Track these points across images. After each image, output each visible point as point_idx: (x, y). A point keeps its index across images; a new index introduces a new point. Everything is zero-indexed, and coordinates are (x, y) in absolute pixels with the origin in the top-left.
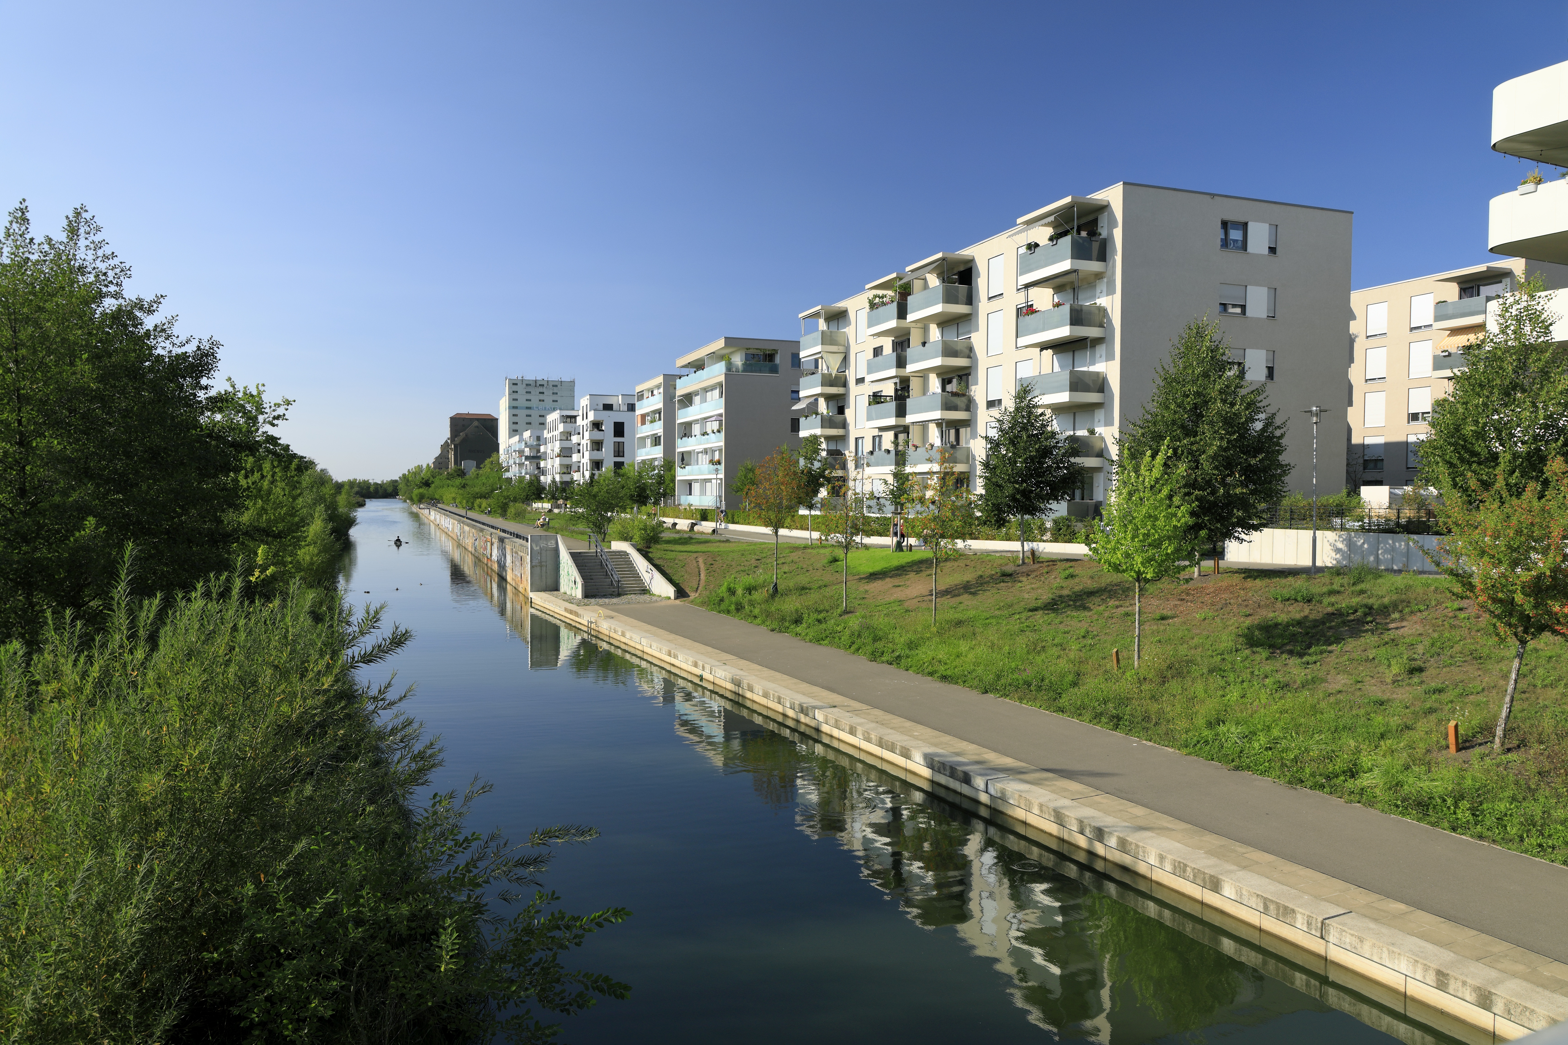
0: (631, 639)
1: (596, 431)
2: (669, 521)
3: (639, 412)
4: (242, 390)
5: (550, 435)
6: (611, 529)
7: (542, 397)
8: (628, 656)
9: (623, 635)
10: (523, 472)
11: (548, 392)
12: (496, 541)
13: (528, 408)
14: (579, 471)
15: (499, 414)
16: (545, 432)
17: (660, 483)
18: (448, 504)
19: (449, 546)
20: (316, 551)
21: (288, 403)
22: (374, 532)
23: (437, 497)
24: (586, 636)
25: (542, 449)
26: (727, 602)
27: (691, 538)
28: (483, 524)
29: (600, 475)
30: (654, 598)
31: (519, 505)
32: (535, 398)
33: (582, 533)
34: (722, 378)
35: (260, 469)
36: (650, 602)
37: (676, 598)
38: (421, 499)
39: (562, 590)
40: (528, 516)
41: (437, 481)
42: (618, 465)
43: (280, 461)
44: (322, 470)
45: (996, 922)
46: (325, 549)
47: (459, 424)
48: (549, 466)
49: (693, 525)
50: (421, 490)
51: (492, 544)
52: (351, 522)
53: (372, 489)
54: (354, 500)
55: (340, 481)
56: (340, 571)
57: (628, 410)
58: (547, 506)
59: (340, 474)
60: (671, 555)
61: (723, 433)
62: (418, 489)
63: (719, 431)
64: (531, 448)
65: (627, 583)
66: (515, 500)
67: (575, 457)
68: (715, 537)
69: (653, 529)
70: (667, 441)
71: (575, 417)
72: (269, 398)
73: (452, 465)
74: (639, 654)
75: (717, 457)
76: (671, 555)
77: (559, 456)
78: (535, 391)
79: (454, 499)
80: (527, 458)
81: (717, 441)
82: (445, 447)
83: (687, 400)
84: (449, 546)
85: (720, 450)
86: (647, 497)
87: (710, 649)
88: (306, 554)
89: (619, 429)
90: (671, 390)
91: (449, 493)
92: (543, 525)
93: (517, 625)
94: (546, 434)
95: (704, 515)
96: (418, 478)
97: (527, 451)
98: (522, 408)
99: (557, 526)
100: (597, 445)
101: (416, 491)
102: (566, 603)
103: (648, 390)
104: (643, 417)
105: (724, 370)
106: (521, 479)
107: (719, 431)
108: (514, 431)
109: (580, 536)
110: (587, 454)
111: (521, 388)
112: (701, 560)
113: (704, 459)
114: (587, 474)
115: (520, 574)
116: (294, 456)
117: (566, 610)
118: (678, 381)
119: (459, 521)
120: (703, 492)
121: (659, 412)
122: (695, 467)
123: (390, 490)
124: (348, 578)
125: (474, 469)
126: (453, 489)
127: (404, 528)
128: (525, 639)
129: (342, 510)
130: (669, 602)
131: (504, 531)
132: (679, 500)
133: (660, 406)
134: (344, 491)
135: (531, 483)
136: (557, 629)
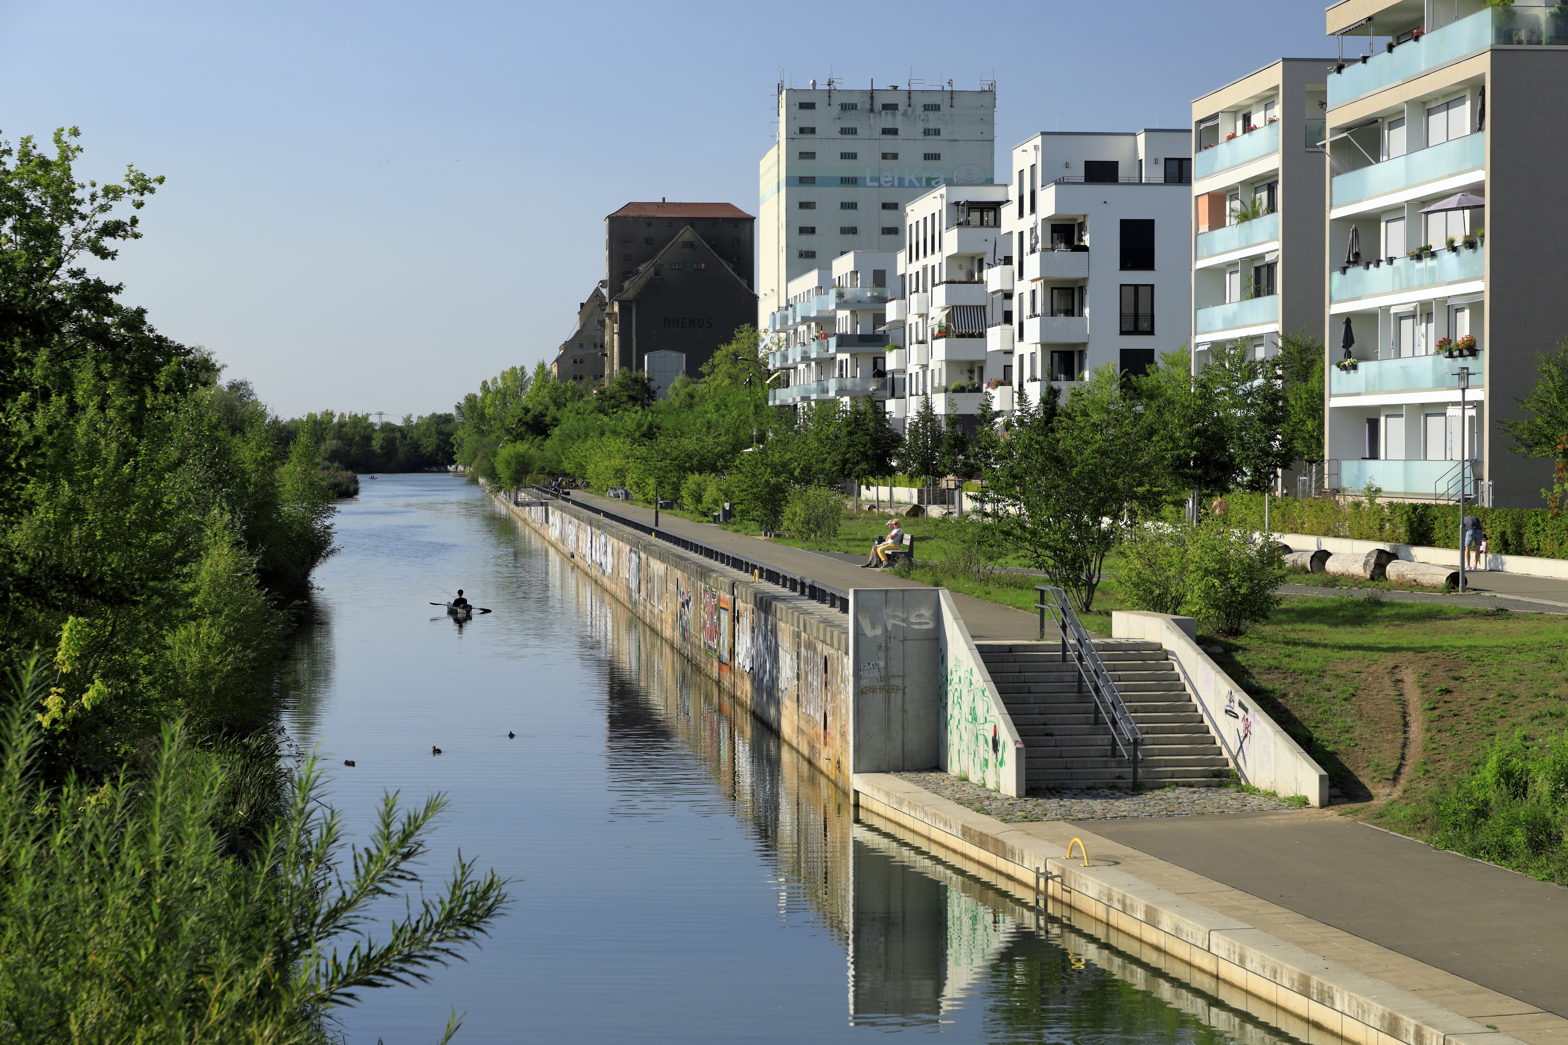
0: (1176, 934)
1: (1062, 254)
2: (1302, 544)
3: (1202, 185)
4: (16, 148)
5: (916, 266)
6: (1113, 570)
7: (889, 144)
8: (1166, 991)
9: (1151, 920)
10: (832, 385)
11: (910, 128)
12: (745, 607)
13: (849, 181)
14: (1006, 381)
15: (757, 203)
16: (902, 257)
17: (1271, 420)
18: (601, 491)
19: (605, 623)
20: (217, 638)
21: (142, 185)
22: (385, 575)
23: (568, 466)
24: (1029, 920)
25: (892, 311)
26: (1498, 820)
27: (1377, 603)
28: (709, 553)
29: (1077, 394)
30: (1254, 802)
31: (820, 494)
32: (868, 148)
33: (1018, 585)
34: (1482, 66)
35: (66, 383)
36: (1241, 813)
37: (1327, 801)
38: (520, 474)
39: (955, 767)
40: (845, 527)
41: (569, 419)
42: (1135, 362)
43: (117, 361)
44: (234, 387)
46: (241, 634)
47: (636, 235)
48: (913, 368)
49: (1383, 559)
50: (521, 447)
51: (736, 618)
52: (316, 547)
53: (376, 445)
54: (325, 477)
55: (285, 417)
56: (284, 691)
57: (1169, 180)
58: (906, 494)
59: (285, 400)
60: (1311, 659)
61: (1485, 250)
62: (511, 443)
63: (1471, 244)
64: (855, 306)
65: (1163, 749)
66: (807, 478)
67: (996, 338)
68: (1458, 601)
69: (1249, 571)
70: (1296, 280)
71: (995, 207)
72: (88, 173)
73: (613, 367)
74: (1205, 984)
75: (1463, 328)
76: (1311, 659)
77: (944, 333)
78: (870, 127)
79: (620, 473)
80: (844, 342)
81: (1465, 278)
82: (592, 310)
83: (1365, 141)
84: (605, 623)
85: (1476, 308)
86: (1229, 468)
87: (1440, 977)
88: (191, 645)
89: (1138, 244)
90: (1310, 110)
91: (605, 455)
92: (892, 559)
93: (812, 877)
94: (903, 265)
95: (1422, 525)
96: (514, 410)
97: (844, 320)
98: (827, 182)
99: (937, 559)
100: (1065, 297)
101: (507, 451)
102: (963, 806)
103: (1233, 112)
104: (1217, 199)
105: (1487, 38)
106: (826, 407)
107: (1471, 244)
108: (803, 257)
109: (1012, 595)
110: (1033, 328)
111: (824, 119)
112: (1409, 677)
113: (1422, 338)
114: (1034, 393)
115: (821, 717)
116: (161, 346)
117: (967, 833)
118: (1333, 79)
119: (635, 546)
120: (1417, 448)
121: (1267, 183)
122: (1391, 366)
123: (429, 445)
124: (306, 726)
125: (679, 379)
126: (614, 444)
127: (471, 566)
128: (837, 925)
129: (291, 508)
130: (1302, 816)
131: (772, 576)
132: (1336, 474)
133: (1274, 162)
134: (296, 451)
135: (856, 421)
136: (936, 894)
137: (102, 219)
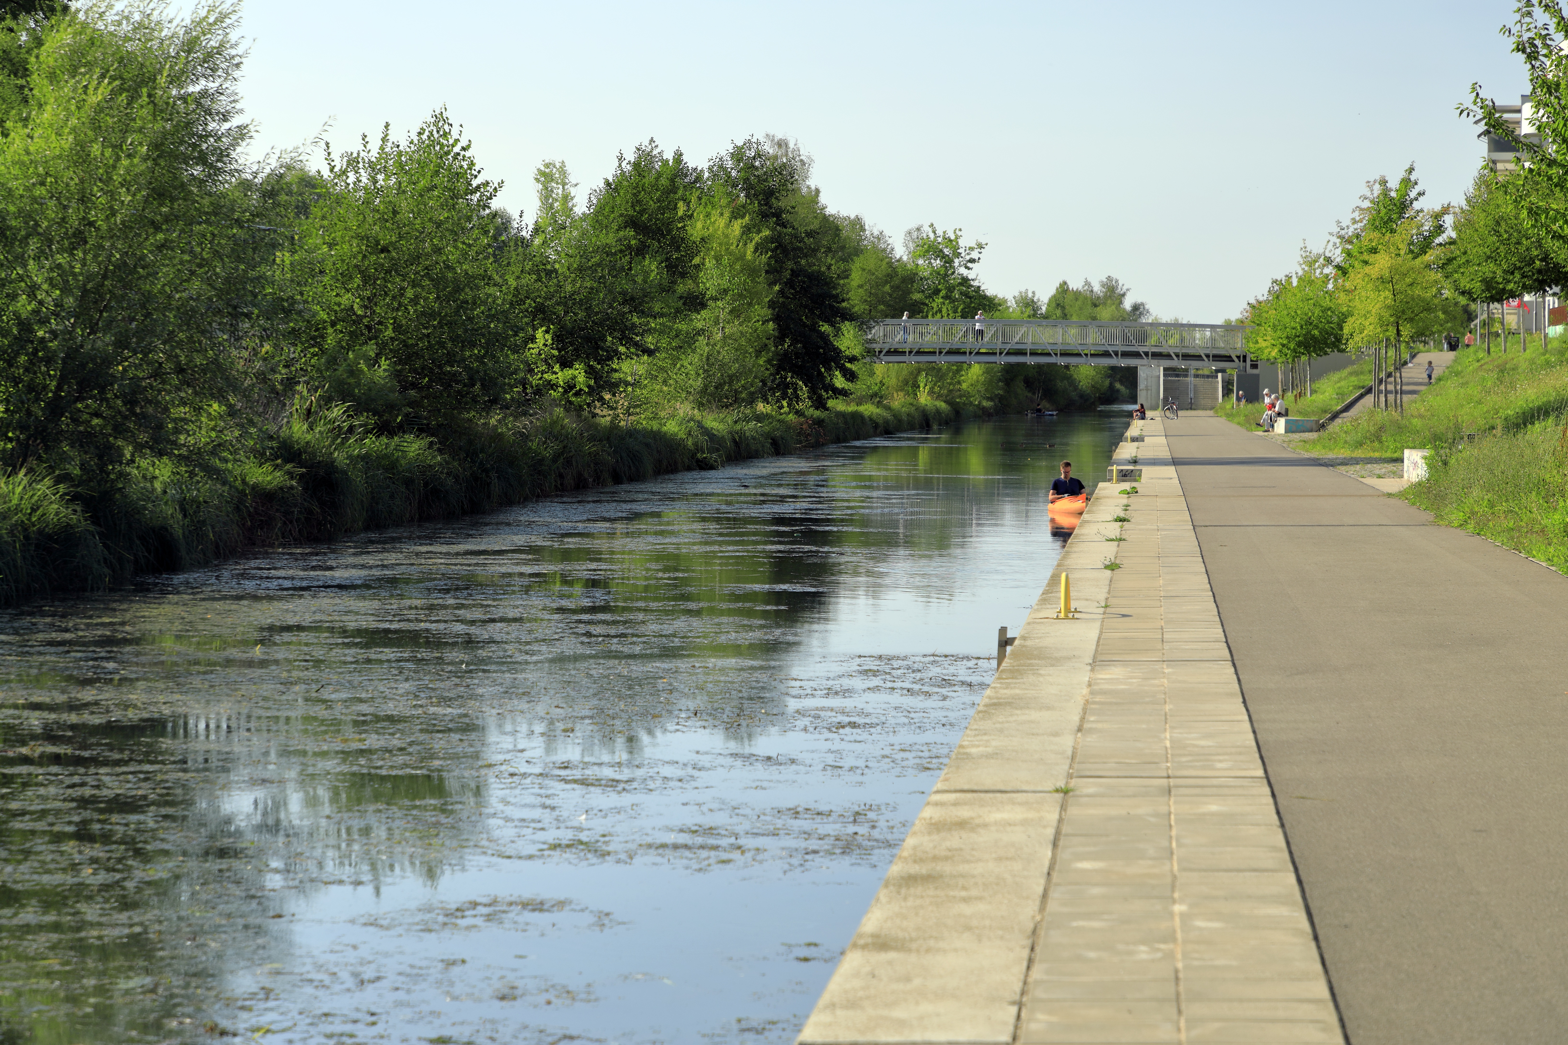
45: (117, 496)
137: (968, 258)
